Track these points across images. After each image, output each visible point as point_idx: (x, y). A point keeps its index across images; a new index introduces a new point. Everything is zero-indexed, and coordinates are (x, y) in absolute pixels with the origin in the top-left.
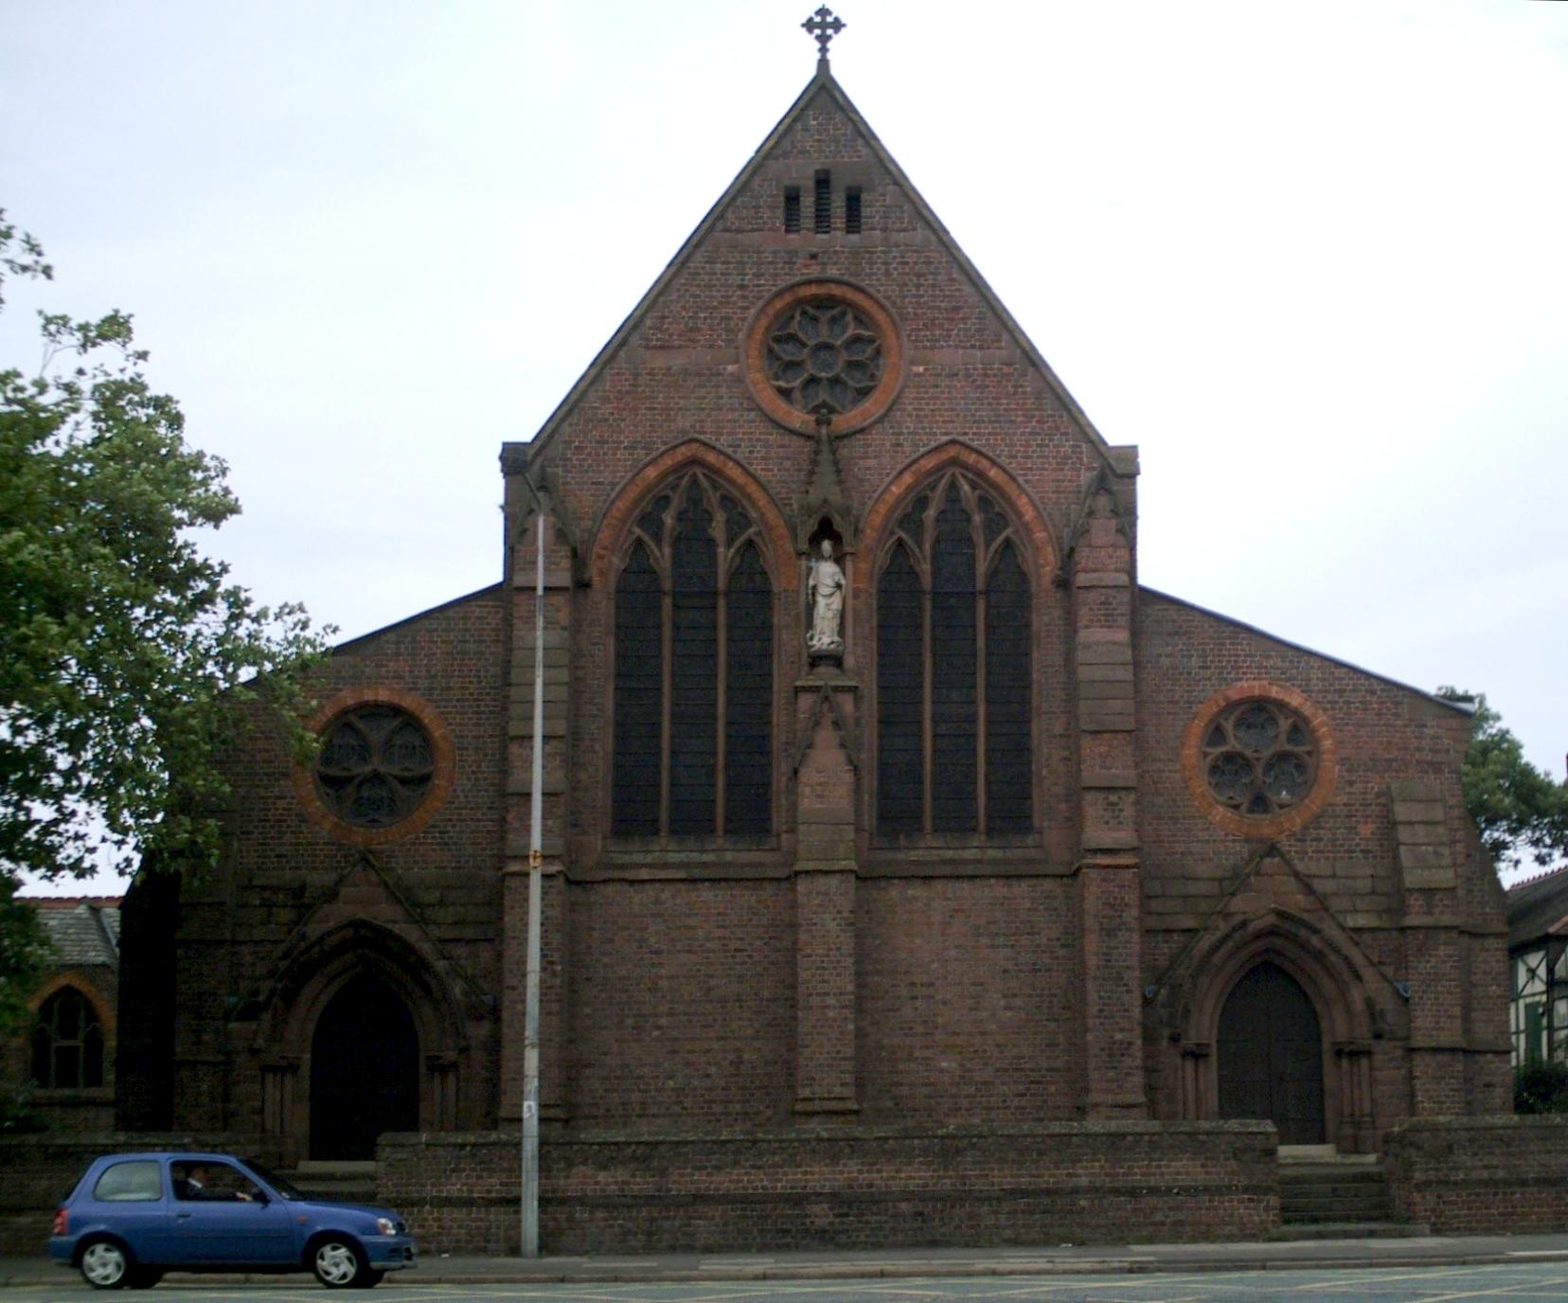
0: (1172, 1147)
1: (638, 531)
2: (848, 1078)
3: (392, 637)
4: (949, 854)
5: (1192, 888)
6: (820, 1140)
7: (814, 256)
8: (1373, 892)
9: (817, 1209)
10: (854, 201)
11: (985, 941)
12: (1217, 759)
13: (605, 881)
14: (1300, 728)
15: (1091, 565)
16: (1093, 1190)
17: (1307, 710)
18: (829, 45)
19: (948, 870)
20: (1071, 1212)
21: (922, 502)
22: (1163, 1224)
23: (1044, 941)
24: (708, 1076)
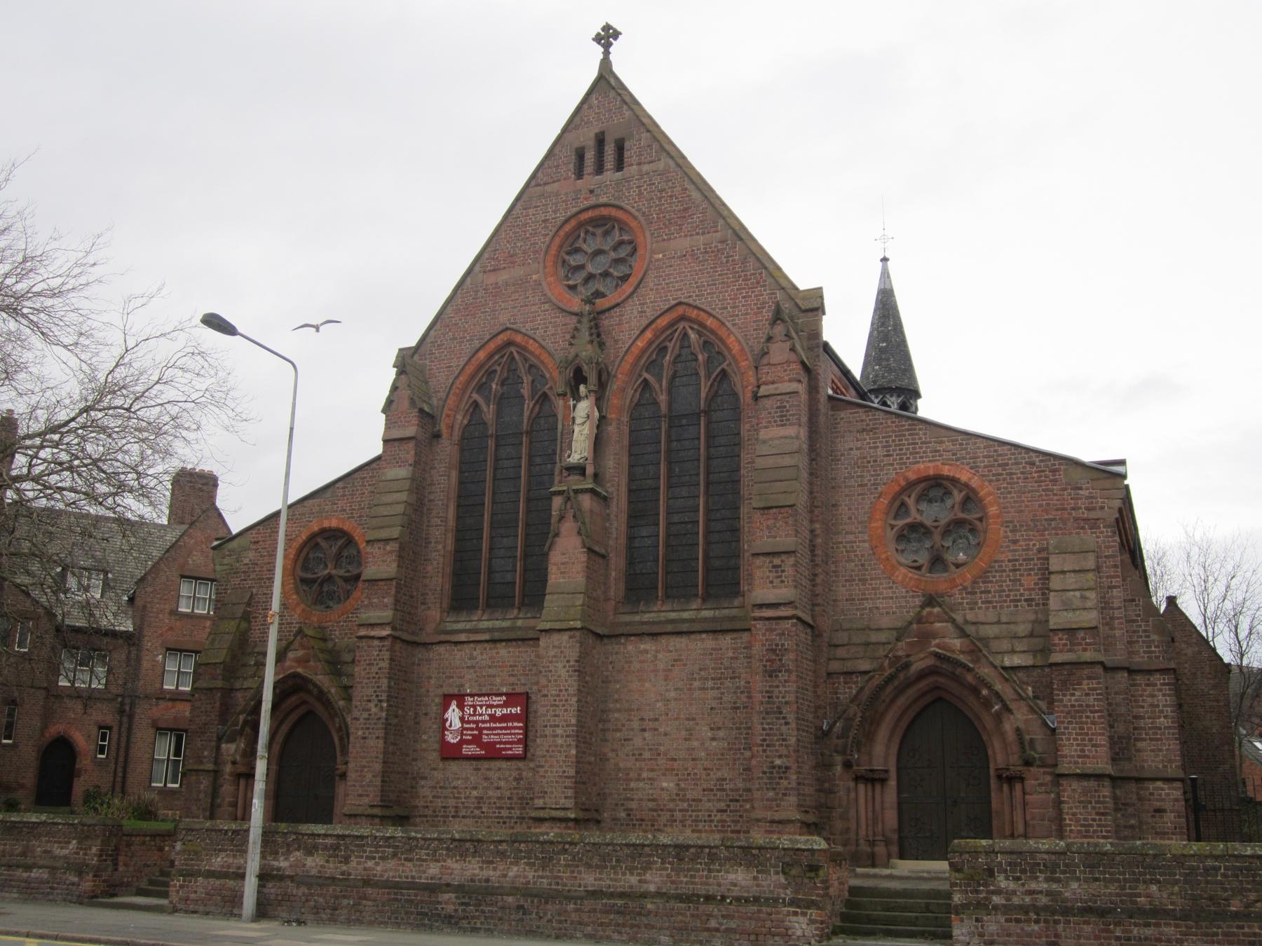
0: (728, 859)
1: (475, 396)
2: (570, 793)
3: (340, 485)
4: (673, 615)
5: (874, 637)
6: (453, 840)
7: (592, 192)
10: (620, 149)
12: (902, 529)
14: (971, 498)
15: (769, 379)
16: (659, 894)
17: (975, 482)
18: (611, 50)
19: (669, 628)
20: (640, 914)
21: (662, 350)
23: (743, 683)
24: (498, 788)
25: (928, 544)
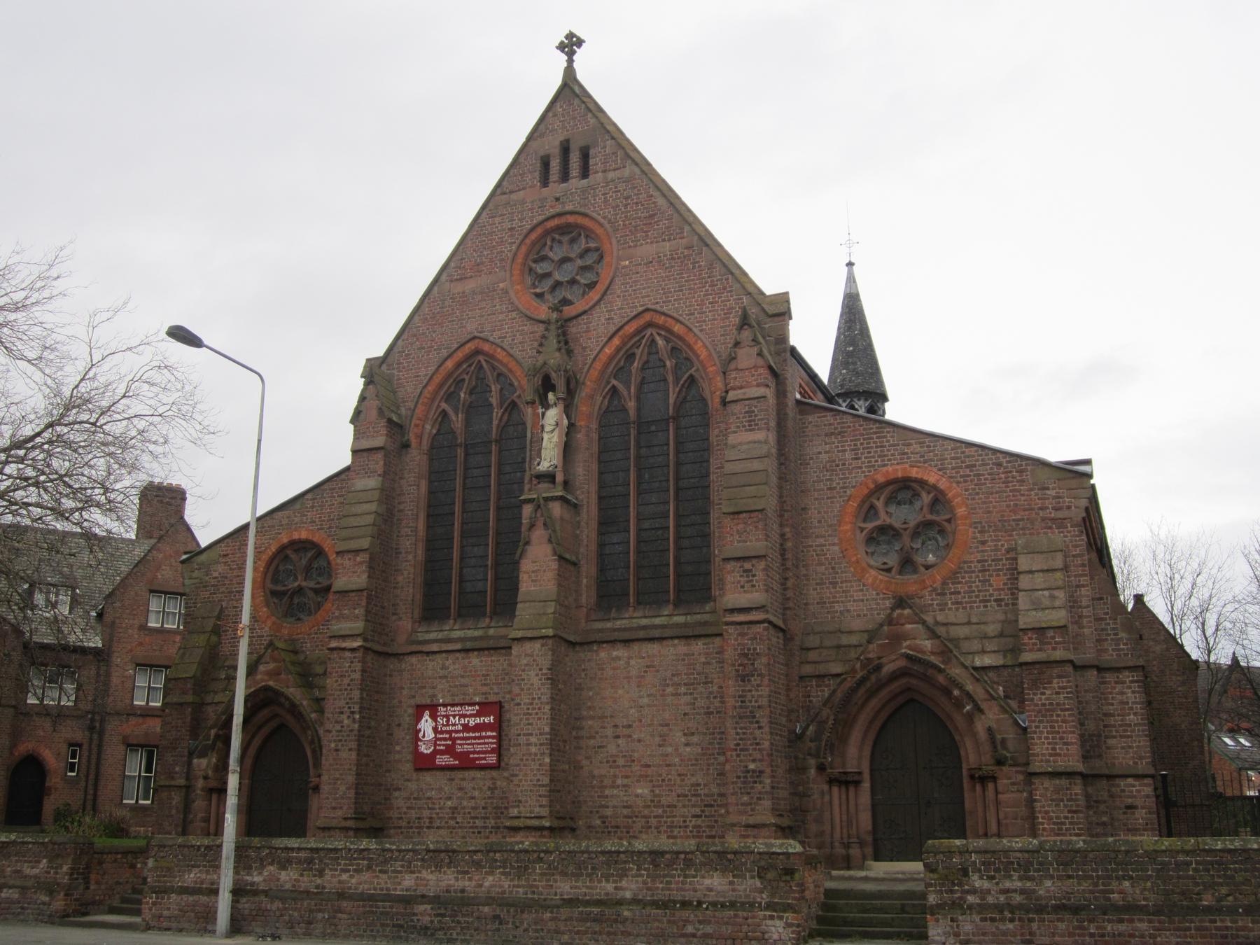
1: (444, 405)
4: (644, 622)
5: (845, 640)
6: (428, 851)
7: (557, 199)
8: (1001, 635)
9: (422, 908)
10: (585, 156)
11: (669, 690)
12: (872, 531)
13: (412, 653)
14: (939, 500)
15: (737, 384)
17: (943, 484)
19: (641, 634)
21: (630, 357)
22: (694, 936)
24: (473, 798)
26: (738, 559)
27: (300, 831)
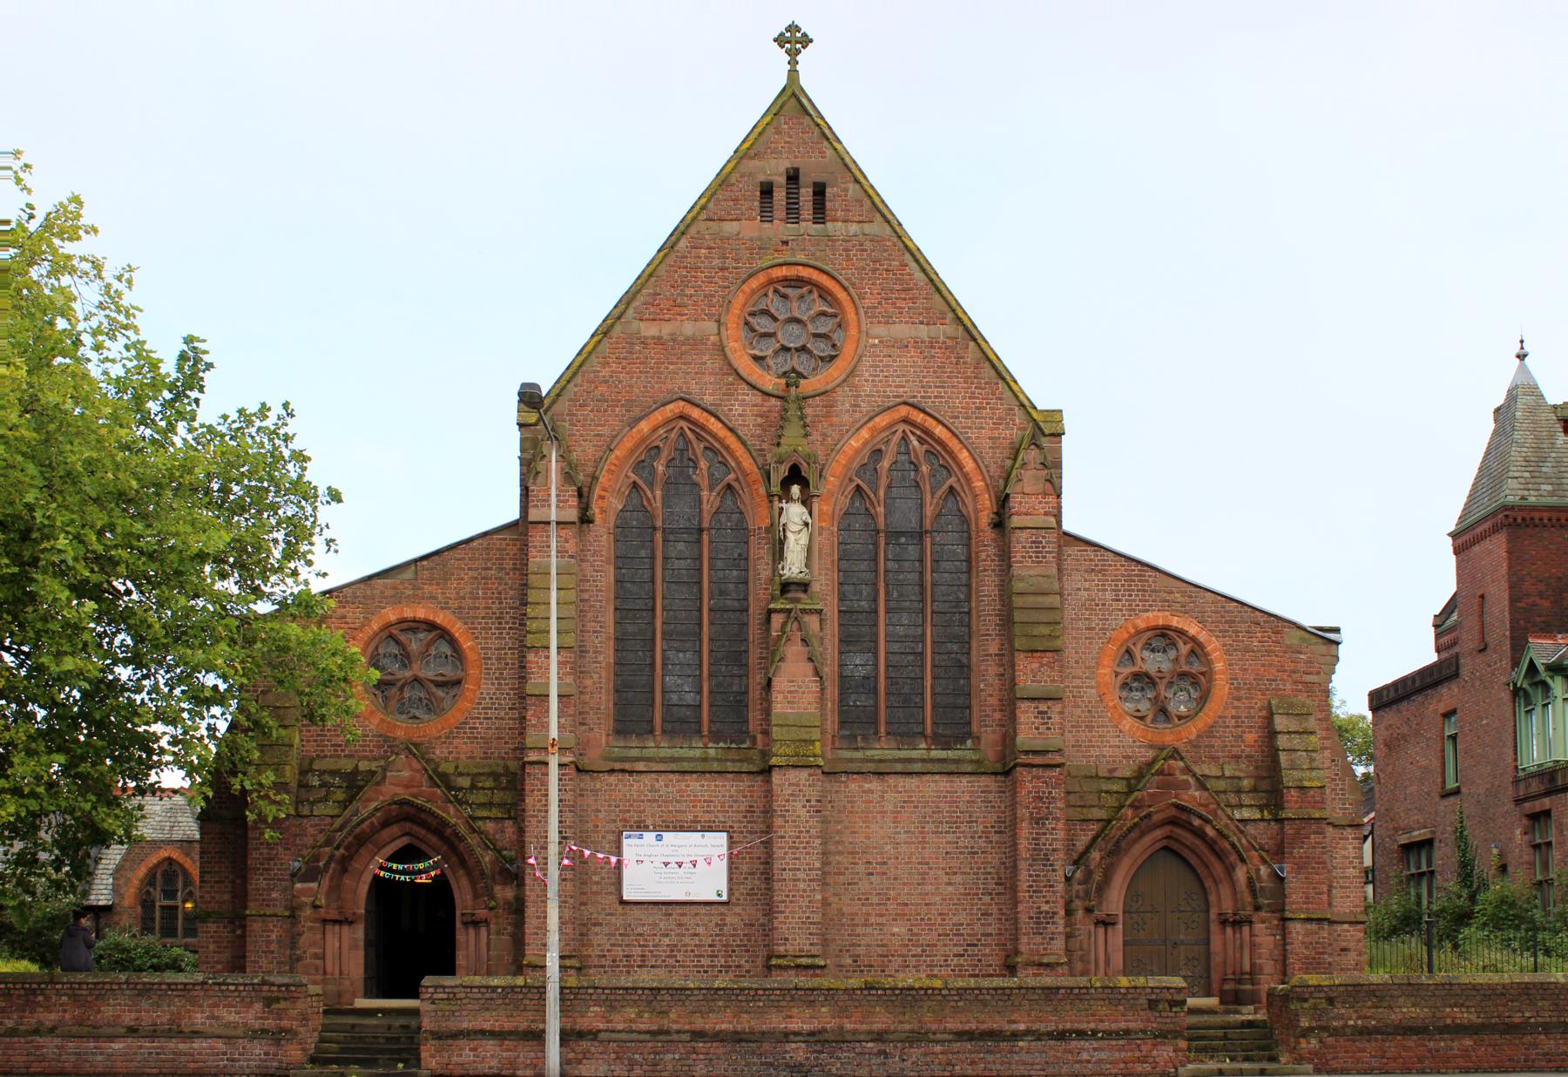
7: (785, 243)
10: (820, 191)
14: (1197, 650)
17: (1203, 637)
19: (899, 767)
21: (877, 453)
22: (1088, 1062)
25: (1150, 695)
26: (1034, 699)
27: (451, 970)
